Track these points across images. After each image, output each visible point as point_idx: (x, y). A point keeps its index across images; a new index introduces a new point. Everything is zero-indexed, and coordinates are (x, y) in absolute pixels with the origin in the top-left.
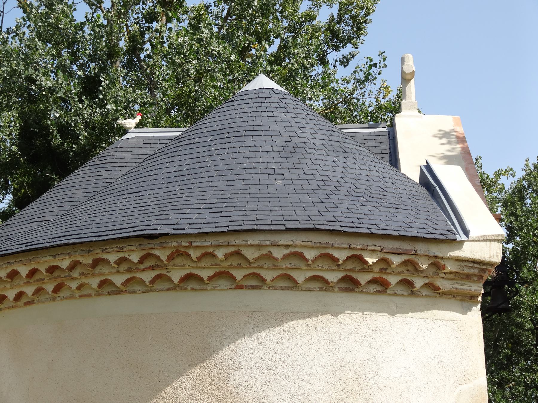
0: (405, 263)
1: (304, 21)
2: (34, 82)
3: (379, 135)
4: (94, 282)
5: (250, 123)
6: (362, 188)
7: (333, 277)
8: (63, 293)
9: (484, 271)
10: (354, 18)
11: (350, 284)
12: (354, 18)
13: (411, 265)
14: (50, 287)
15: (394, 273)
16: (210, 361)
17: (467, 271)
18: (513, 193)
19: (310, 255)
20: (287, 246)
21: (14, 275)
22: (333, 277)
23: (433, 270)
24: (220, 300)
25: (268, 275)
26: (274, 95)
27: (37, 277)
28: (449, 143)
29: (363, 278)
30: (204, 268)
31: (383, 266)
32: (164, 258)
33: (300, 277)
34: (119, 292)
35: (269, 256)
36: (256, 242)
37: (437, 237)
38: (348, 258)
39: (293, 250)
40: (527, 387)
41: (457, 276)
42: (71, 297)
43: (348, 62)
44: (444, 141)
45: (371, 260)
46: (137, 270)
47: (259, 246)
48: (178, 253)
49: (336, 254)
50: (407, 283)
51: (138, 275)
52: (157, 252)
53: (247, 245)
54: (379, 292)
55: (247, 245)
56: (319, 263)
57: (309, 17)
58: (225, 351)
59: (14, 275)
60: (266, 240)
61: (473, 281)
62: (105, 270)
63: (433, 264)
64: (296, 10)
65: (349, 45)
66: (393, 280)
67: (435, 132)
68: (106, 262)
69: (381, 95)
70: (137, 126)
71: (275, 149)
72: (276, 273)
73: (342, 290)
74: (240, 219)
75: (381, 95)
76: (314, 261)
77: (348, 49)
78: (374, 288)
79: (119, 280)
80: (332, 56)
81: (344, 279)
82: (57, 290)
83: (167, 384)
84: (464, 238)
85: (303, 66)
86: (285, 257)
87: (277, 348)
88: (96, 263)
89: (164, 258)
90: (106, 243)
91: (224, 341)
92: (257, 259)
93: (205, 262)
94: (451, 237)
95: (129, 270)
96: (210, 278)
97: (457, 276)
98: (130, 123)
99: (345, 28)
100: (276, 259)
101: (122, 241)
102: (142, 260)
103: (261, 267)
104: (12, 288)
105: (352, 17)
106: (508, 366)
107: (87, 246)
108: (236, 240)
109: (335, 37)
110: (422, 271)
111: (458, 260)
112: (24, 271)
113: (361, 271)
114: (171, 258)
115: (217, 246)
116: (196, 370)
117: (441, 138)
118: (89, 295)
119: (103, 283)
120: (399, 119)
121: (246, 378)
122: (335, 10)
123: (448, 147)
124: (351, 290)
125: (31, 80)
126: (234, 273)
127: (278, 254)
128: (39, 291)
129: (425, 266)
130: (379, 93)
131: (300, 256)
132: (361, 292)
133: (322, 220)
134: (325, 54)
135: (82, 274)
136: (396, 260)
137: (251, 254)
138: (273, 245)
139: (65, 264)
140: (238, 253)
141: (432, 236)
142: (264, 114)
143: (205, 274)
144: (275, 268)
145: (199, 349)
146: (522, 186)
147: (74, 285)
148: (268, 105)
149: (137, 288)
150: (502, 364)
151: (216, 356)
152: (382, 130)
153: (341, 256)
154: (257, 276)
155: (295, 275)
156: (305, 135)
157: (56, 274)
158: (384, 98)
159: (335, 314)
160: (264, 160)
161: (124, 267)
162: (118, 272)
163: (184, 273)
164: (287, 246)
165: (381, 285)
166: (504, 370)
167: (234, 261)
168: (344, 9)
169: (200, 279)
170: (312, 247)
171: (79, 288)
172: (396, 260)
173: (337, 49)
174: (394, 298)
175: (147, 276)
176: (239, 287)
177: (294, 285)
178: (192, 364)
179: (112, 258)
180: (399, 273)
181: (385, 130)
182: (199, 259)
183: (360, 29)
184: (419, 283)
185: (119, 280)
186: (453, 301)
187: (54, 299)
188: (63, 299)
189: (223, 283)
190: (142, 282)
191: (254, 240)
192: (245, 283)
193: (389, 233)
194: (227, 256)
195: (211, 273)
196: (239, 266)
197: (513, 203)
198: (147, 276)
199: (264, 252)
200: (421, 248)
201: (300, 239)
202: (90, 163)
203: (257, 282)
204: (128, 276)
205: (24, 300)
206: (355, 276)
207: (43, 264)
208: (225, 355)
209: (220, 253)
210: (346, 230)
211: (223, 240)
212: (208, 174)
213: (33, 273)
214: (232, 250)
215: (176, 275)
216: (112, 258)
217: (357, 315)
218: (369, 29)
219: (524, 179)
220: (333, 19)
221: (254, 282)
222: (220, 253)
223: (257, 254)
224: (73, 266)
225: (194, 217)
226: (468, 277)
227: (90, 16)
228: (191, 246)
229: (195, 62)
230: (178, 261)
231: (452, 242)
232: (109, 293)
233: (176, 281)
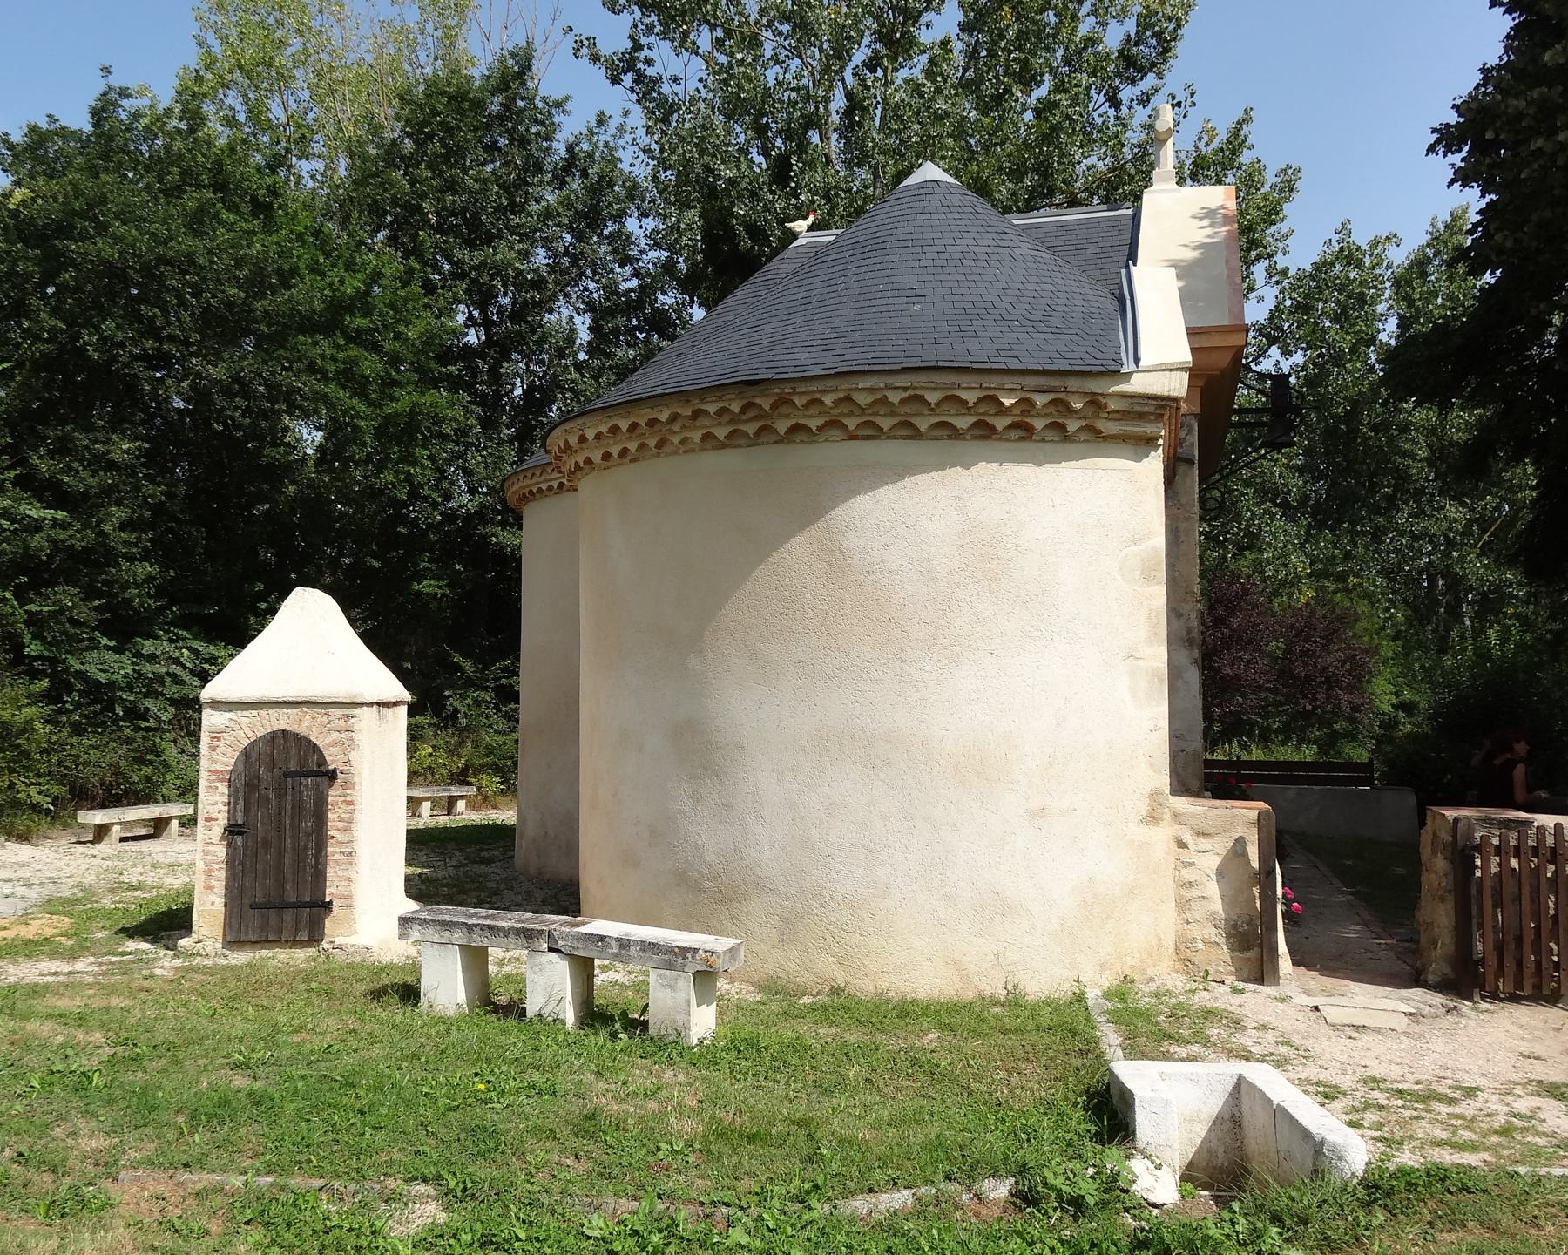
0: (1054, 402)
1: (1085, 48)
2: (711, 171)
3: (1119, 219)
4: (696, 436)
5: (900, 231)
6: (1022, 307)
7: (963, 422)
8: (665, 450)
9: (1164, 407)
10: (1159, 35)
11: (984, 431)
12: (1159, 35)
13: (1061, 405)
14: (652, 442)
15: (1039, 415)
16: (821, 523)
17: (1138, 409)
18: (1411, 266)
19: (932, 397)
20: (905, 389)
21: (615, 429)
22: (963, 422)
23: (1091, 409)
24: (834, 453)
25: (886, 423)
26: (937, 190)
27: (638, 431)
28: (1212, 225)
29: (1000, 423)
30: (812, 416)
31: (1024, 407)
32: (767, 408)
33: (923, 424)
34: (723, 446)
35: (884, 401)
36: (869, 385)
37: (1093, 369)
38: (979, 400)
39: (911, 392)
40: (1415, 537)
41: (1124, 415)
42: (676, 453)
43: (1148, 100)
44: (1206, 222)
45: (1007, 402)
46: (740, 421)
47: (871, 390)
48: (783, 402)
49: (964, 395)
50: (1061, 427)
51: (742, 427)
52: (758, 401)
53: (857, 389)
54: (1022, 439)
55: (857, 389)
56: (945, 407)
57: (1091, 41)
58: (838, 511)
59: (615, 429)
60: (879, 382)
61: (1150, 421)
62: (707, 422)
63: (1092, 402)
64: (1074, 30)
65: (1151, 76)
66: (1039, 424)
67: (1196, 210)
68: (705, 412)
69: (1203, 142)
70: (810, 229)
71: (923, 263)
72: (895, 421)
73: (975, 438)
74: (855, 358)
75: (1203, 142)
76: (938, 404)
77: (1150, 80)
78: (1014, 434)
79: (721, 433)
80: (1126, 93)
81: (975, 425)
82: (660, 445)
83: (776, 549)
84: (1132, 368)
85: (1068, 117)
86: (902, 402)
87: (896, 506)
88: (697, 414)
89: (767, 408)
90: (704, 392)
91: (837, 499)
92: (871, 405)
93: (813, 411)
94: (1112, 368)
95: (731, 422)
96: (820, 429)
97: (1124, 415)
98: (800, 226)
99: (1147, 51)
100: (892, 404)
101: (720, 389)
102: (744, 410)
103: (877, 414)
104: (696, 428)
105: (1154, 35)
106: (1388, 509)
107: (683, 396)
108: (845, 384)
109: (1131, 64)
110: (1077, 411)
111: (1124, 396)
112: (624, 425)
113: (996, 414)
114: (774, 406)
115: (825, 391)
116: (806, 532)
117: (1201, 219)
118: (693, 451)
119: (707, 437)
120: (1148, 197)
121: (861, 542)
122: (1131, 26)
123: (1209, 231)
124: (988, 438)
125: (709, 170)
126: (846, 421)
127: (895, 397)
128: (642, 446)
129: (1079, 406)
130: (1200, 139)
131: (921, 399)
132: (1000, 439)
133: (949, 355)
134: (1116, 90)
135: (683, 427)
136: (1040, 400)
137: (863, 399)
138: (889, 387)
139: (664, 417)
140: (848, 399)
141: (1088, 369)
142: (920, 217)
143: (814, 424)
144: (893, 414)
145: (810, 509)
146: (1424, 254)
147: (676, 440)
148: (926, 204)
149: (742, 442)
150: (1380, 507)
151: (828, 517)
152: (1126, 212)
153: (971, 397)
154: (874, 425)
155: (917, 421)
156: (965, 242)
157: (657, 427)
158: (1207, 145)
159: (967, 467)
160: (906, 279)
161: (726, 418)
162: (720, 424)
163: (790, 423)
164: (905, 389)
165: (1024, 430)
166: (1381, 515)
167: (844, 409)
168: (1145, 22)
169: (807, 429)
170: (934, 389)
171: (682, 442)
172: (1040, 400)
173: (1133, 82)
174: (1041, 445)
175: (751, 428)
176: (853, 437)
177: (916, 434)
178: (803, 527)
179: (712, 408)
180: (1046, 415)
181: (1130, 212)
182: (806, 406)
183: (1166, 50)
184: (1072, 426)
185: (721, 433)
186: (1122, 446)
187: (658, 455)
188: (667, 455)
189: (836, 434)
190: (745, 434)
191: (867, 382)
192: (860, 433)
193: (1030, 367)
194: (837, 403)
195: (820, 422)
196: (851, 414)
197: (1409, 282)
198: (751, 428)
199: (879, 396)
200: (1073, 384)
201: (920, 380)
202: (752, 280)
203: (872, 432)
204: (730, 428)
205: (630, 457)
206: (990, 420)
207: (643, 416)
208: (839, 515)
209: (828, 400)
210: (975, 366)
211: (830, 384)
212: (837, 300)
213: (633, 427)
214: (842, 395)
215: (782, 427)
216: (712, 408)
217: (995, 466)
218: (1180, 48)
219: (1428, 245)
220: (1129, 40)
221: (869, 432)
222: (828, 400)
223: (870, 399)
224: (674, 418)
225: (803, 357)
226: (1141, 416)
227: (780, 78)
228: (795, 393)
229: (916, 127)
230: (784, 409)
231: (1116, 374)
232: (714, 448)
233: (782, 433)
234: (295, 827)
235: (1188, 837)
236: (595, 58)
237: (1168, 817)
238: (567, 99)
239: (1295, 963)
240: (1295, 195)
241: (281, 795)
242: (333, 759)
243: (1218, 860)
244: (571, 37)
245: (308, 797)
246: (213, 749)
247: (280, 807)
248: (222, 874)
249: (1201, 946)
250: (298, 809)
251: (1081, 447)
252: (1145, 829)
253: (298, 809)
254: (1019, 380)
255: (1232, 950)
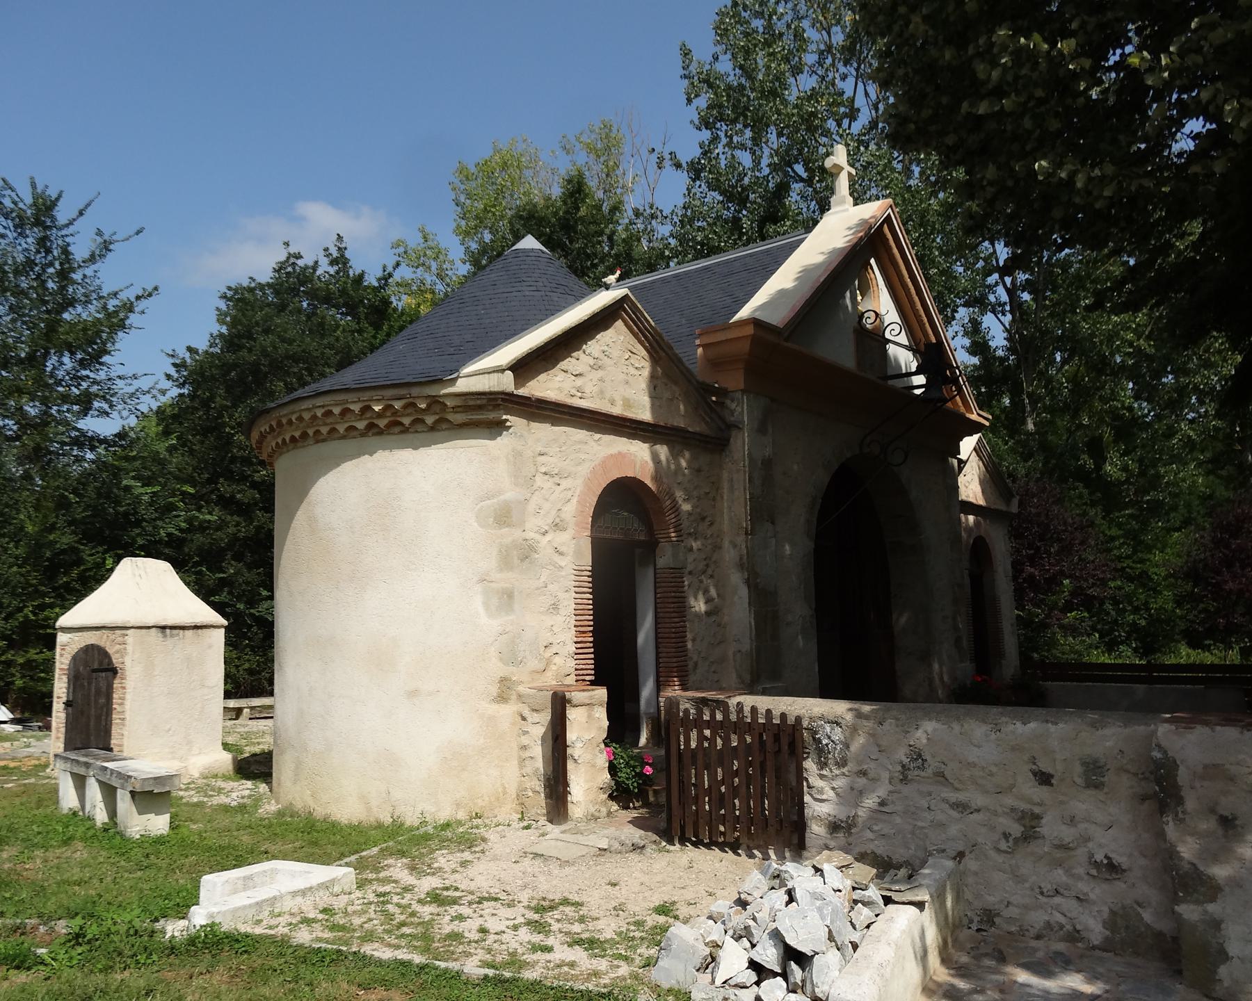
20: (323, 406)
24: (312, 451)
34: (343, 437)
41: (455, 409)
159: (416, 448)
163: (347, 425)
200: (415, 391)
203: (319, 439)
217: (387, 453)
226: (480, 408)
232: (402, 432)
234: (96, 702)
235: (526, 713)
236: (678, 166)
237: (514, 697)
238: (99, 233)
239: (620, 794)
240: (110, 255)
241: (89, 684)
242: (116, 660)
243: (543, 730)
244: (655, 155)
245: (103, 685)
246: (62, 655)
247: (89, 689)
248: (63, 730)
249: (530, 794)
250: (98, 692)
251: (446, 433)
252: (495, 707)
253: (98, 692)
254: (360, 394)
255: (546, 797)
